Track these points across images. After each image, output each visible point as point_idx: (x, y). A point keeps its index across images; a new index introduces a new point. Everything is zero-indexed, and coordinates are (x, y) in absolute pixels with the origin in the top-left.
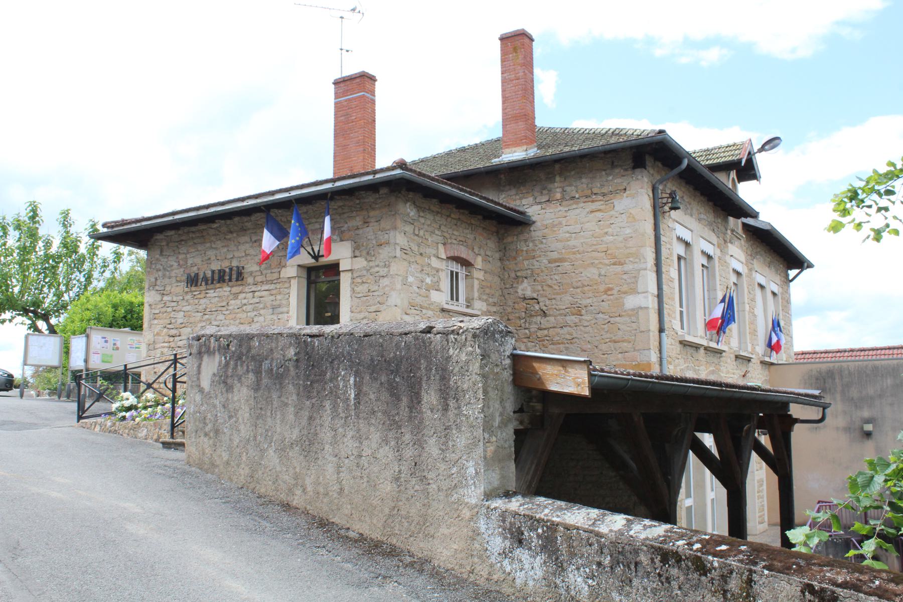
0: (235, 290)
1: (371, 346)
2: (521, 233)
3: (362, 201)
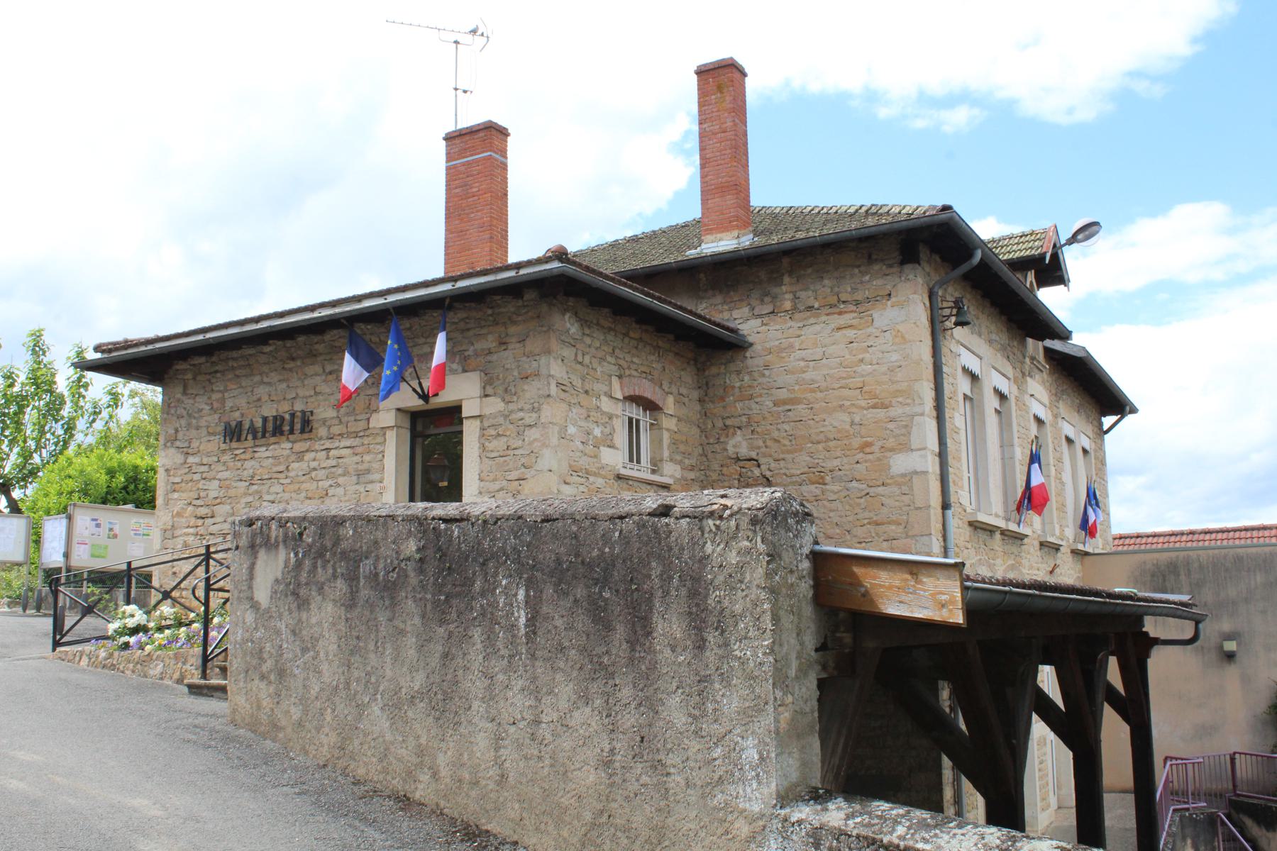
0: (299, 446)
1: (555, 537)
2: (732, 360)
3: (497, 310)
